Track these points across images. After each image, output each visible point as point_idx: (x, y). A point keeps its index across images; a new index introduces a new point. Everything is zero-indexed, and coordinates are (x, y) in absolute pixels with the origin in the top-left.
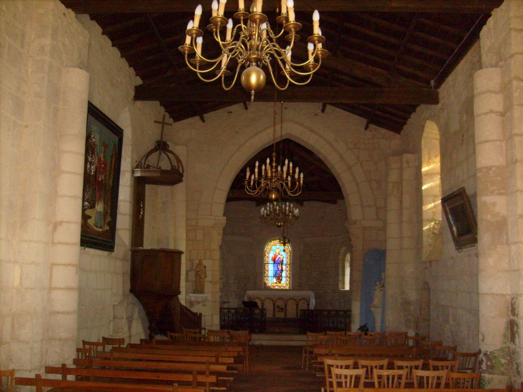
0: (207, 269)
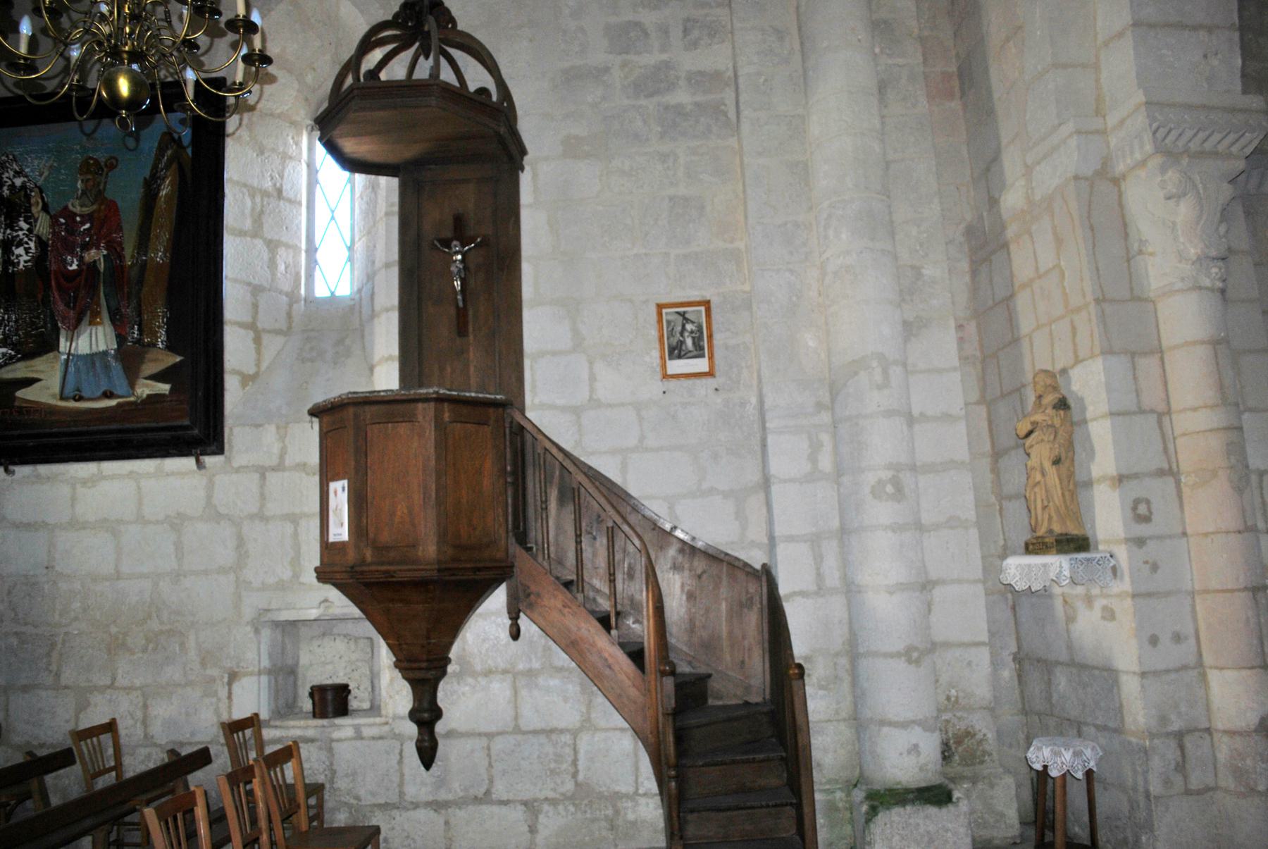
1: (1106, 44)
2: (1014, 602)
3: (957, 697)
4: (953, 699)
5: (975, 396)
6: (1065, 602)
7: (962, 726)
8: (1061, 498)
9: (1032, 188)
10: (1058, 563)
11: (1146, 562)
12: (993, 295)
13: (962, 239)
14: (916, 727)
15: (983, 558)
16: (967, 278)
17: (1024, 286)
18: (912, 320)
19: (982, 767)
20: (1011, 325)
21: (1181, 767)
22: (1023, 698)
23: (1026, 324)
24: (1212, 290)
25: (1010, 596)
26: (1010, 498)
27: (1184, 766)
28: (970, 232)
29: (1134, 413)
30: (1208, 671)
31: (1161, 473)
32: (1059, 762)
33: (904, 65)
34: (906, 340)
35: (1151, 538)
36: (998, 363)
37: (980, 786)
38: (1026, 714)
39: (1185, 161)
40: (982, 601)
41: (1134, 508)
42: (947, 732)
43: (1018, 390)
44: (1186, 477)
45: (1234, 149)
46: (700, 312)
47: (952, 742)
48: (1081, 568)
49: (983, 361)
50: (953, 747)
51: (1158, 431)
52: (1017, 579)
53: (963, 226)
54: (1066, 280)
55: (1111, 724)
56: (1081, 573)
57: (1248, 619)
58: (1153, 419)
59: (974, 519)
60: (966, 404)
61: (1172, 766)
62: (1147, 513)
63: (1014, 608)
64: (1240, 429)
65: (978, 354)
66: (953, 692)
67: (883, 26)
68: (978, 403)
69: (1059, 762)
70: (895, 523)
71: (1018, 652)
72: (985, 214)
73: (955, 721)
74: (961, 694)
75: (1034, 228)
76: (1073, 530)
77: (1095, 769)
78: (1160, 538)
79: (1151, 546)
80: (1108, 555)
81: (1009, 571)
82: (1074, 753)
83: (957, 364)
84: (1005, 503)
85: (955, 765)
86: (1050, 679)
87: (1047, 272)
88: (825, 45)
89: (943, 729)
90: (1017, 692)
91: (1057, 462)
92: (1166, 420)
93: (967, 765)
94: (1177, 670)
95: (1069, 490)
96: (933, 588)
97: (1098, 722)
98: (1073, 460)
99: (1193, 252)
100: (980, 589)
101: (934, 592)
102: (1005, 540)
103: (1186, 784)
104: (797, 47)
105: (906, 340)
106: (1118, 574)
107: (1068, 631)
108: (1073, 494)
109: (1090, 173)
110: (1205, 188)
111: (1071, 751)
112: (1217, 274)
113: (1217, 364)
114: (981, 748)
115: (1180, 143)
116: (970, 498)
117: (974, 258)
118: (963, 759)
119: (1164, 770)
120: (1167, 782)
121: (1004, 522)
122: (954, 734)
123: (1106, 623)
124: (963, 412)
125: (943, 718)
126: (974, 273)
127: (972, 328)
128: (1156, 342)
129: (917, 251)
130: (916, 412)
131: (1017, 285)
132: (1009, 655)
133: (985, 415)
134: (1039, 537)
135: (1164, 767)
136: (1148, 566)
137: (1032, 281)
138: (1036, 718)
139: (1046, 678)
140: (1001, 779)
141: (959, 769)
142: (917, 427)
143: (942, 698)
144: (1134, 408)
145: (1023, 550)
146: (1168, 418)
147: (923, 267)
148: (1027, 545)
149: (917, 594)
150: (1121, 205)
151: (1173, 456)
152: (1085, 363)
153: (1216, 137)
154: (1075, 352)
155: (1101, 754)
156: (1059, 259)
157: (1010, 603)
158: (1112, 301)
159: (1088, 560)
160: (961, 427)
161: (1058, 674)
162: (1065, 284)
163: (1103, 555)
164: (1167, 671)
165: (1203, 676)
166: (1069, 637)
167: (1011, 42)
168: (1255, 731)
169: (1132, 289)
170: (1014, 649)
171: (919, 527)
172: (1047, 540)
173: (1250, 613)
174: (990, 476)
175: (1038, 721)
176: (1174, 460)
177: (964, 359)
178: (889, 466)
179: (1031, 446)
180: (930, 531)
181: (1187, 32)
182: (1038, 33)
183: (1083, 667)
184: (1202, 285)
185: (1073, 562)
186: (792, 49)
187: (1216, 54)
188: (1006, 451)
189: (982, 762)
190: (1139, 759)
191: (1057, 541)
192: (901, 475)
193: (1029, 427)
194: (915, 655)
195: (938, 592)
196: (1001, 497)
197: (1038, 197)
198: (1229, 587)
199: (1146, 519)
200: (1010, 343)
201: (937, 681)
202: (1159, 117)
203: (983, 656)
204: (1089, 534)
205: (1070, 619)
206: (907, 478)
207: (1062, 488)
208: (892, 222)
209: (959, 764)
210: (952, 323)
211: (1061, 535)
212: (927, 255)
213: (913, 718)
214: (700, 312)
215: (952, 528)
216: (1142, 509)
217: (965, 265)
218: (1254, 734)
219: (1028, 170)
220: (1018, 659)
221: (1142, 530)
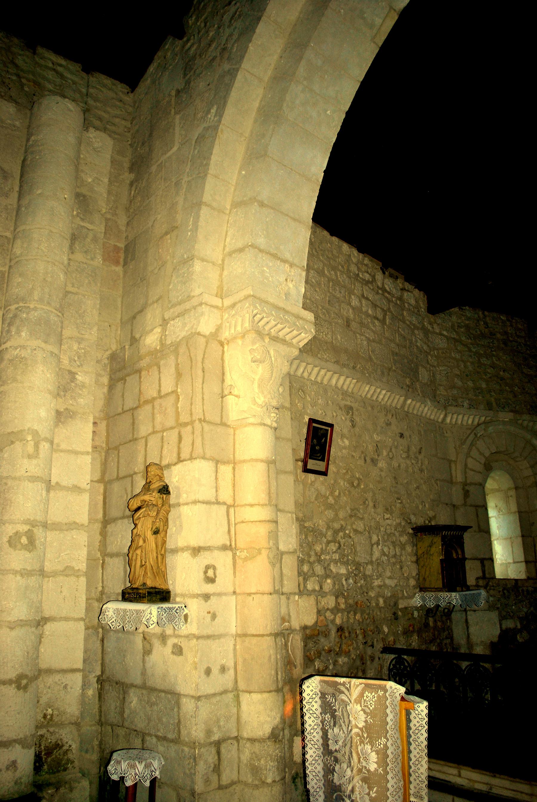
0: (173, 499)
1: (230, 254)
2: (103, 636)
3: (52, 715)
4: (49, 717)
5: (97, 476)
6: (145, 638)
7: (52, 739)
8: (156, 559)
9: (166, 336)
10: (149, 610)
11: (209, 613)
12: (123, 405)
13: (106, 361)
14: (17, 745)
15: (87, 599)
16: (105, 390)
17: (147, 402)
18: (62, 410)
19: (66, 773)
20: (133, 428)
21: (217, 769)
22: (100, 712)
23: (144, 430)
24: (271, 427)
25: (100, 630)
26: (112, 555)
27: (219, 768)
28: (113, 357)
29: (213, 503)
30: (241, 693)
31: (224, 548)
32: (133, 774)
33: (92, 230)
34: (56, 425)
35: (214, 594)
36: (118, 454)
37: (62, 790)
38: (102, 725)
39: (267, 340)
40: (81, 636)
41: (206, 572)
42: (40, 745)
43: (131, 476)
44: (240, 552)
45: (295, 341)
46: (328, 430)
47: (43, 753)
48: (165, 615)
49: (107, 452)
50: (44, 757)
51: (226, 518)
52: (113, 620)
53: (109, 352)
54: (180, 403)
55: (170, 736)
56: (164, 619)
57: (270, 657)
58: (224, 508)
59: (85, 571)
60: (92, 481)
61: (211, 769)
62: (213, 576)
63: (102, 641)
64: (276, 522)
65: (104, 445)
66: (50, 711)
67: (81, 198)
68: (98, 481)
69: (133, 774)
70: (24, 569)
71: (102, 675)
72: (127, 347)
73: (48, 735)
74: (56, 712)
75: (162, 362)
76: (159, 584)
77: (159, 777)
78: (220, 595)
79: (213, 600)
80: (183, 606)
81: (107, 613)
82: (145, 765)
83: (90, 450)
84: (107, 559)
85: (44, 773)
86: (124, 698)
87: (167, 394)
88: (39, 192)
89: (37, 743)
90: (97, 706)
91: (156, 532)
92: (232, 510)
93: (54, 773)
94: (221, 693)
95: (161, 555)
96: (46, 623)
97: (160, 734)
98: (166, 532)
99: (261, 400)
100: (81, 626)
101: (45, 627)
102: (103, 587)
103: (219, 781)
104: (17, 188)
105: (56, 425)
106: (189, 620)
107: (144, 661)
108: (163, 556)
109: (208, 333)
110: (276, 360)
111: (144, 763)
112: (275, 417)
113: (269, 476)
114: (66, 757)
115: (267, 328)
116: (83, 553)
117: (113, 376)
118: (50, 767)
119: (206, 772)
120: (207, 781)
121: (104, 573)
122: (45, 747)
123: (175, 656)
124: (88, 487)
125: (39, 734)
126: (111, 387)
127: (103, 426)
128: (232, 456)
129: (75, 361)
130: (53, 483)
131: (142, 400)
132: (95, 677)
133: (102, 490)
134: (135, 588)
135: (205, 769)
136: (210, 615)
137: (154, 399)
138: (109, 728)
139: (121, 697)
140: (79, 783)
141: (47, 776)
142: (52, 494)
143: (40, 717)
144: (213, 500)
145: (120, 598)
146: (233, 509)
147: (77, 374)
148: (124, 593)
149: (34, 629)
150: (223, 360)
151: (233, 536)
152: (185, 462)
153: (287, 330)
154: (179, 454)
155: (163, 763)
156: (177, 388)
157: (100, 636)
158: (209, 423)
159: (170, 609)
160: (86, 497)
161: (131, 694)
162: (179, 405)
163: (180, 606)
164: (214, 695)
165: (237, 697)
166: (144, 666)
167: (169, 236)
168: (269, 738)
169: (222, 418)
170: (99, 673)
171: (42, 573)
172: (141, 591)
173: (272, 652)
174: (98, 538)
175: (110, 731)
176: (233, 540)
177: (94, 447)
178: (27, 522)
179: (139, 518)
180: (49, 577)
181: (279, 261)
182: (189, 234)
183: (153, 690)
184: (266, 423)
185: (159, 610)
186: (13, 188)
187: (292, 281)
188: (115, 520)
189: (65, 769)
190: (189, 764)
191: (149, 593)
192: (35, 530)
193: (139, 504)
194: (24, 682)
195: (48, 628)
196: (105, 554)
197: (168, 342)
198: (261, 633)
199: (211, 580)
200: (130, 441)
201: (38, 702)
202: (259, 307)
203: (79, 677)
204: (171, 588)
205: (147, 652)
206: (39, 532)
207: (157, 553)
208: (61, 335)
209: (47, 773)
210: (91, 419)
211: (152, 588)
212: (82, 365)
213: (15, 738)
214: (328, 430)
215: (67, 576)
216: (210, 573)
217: (105, 380)
218: (267, 741)
219: (165, 323)
220: (100, 680)
221: (209, 588)
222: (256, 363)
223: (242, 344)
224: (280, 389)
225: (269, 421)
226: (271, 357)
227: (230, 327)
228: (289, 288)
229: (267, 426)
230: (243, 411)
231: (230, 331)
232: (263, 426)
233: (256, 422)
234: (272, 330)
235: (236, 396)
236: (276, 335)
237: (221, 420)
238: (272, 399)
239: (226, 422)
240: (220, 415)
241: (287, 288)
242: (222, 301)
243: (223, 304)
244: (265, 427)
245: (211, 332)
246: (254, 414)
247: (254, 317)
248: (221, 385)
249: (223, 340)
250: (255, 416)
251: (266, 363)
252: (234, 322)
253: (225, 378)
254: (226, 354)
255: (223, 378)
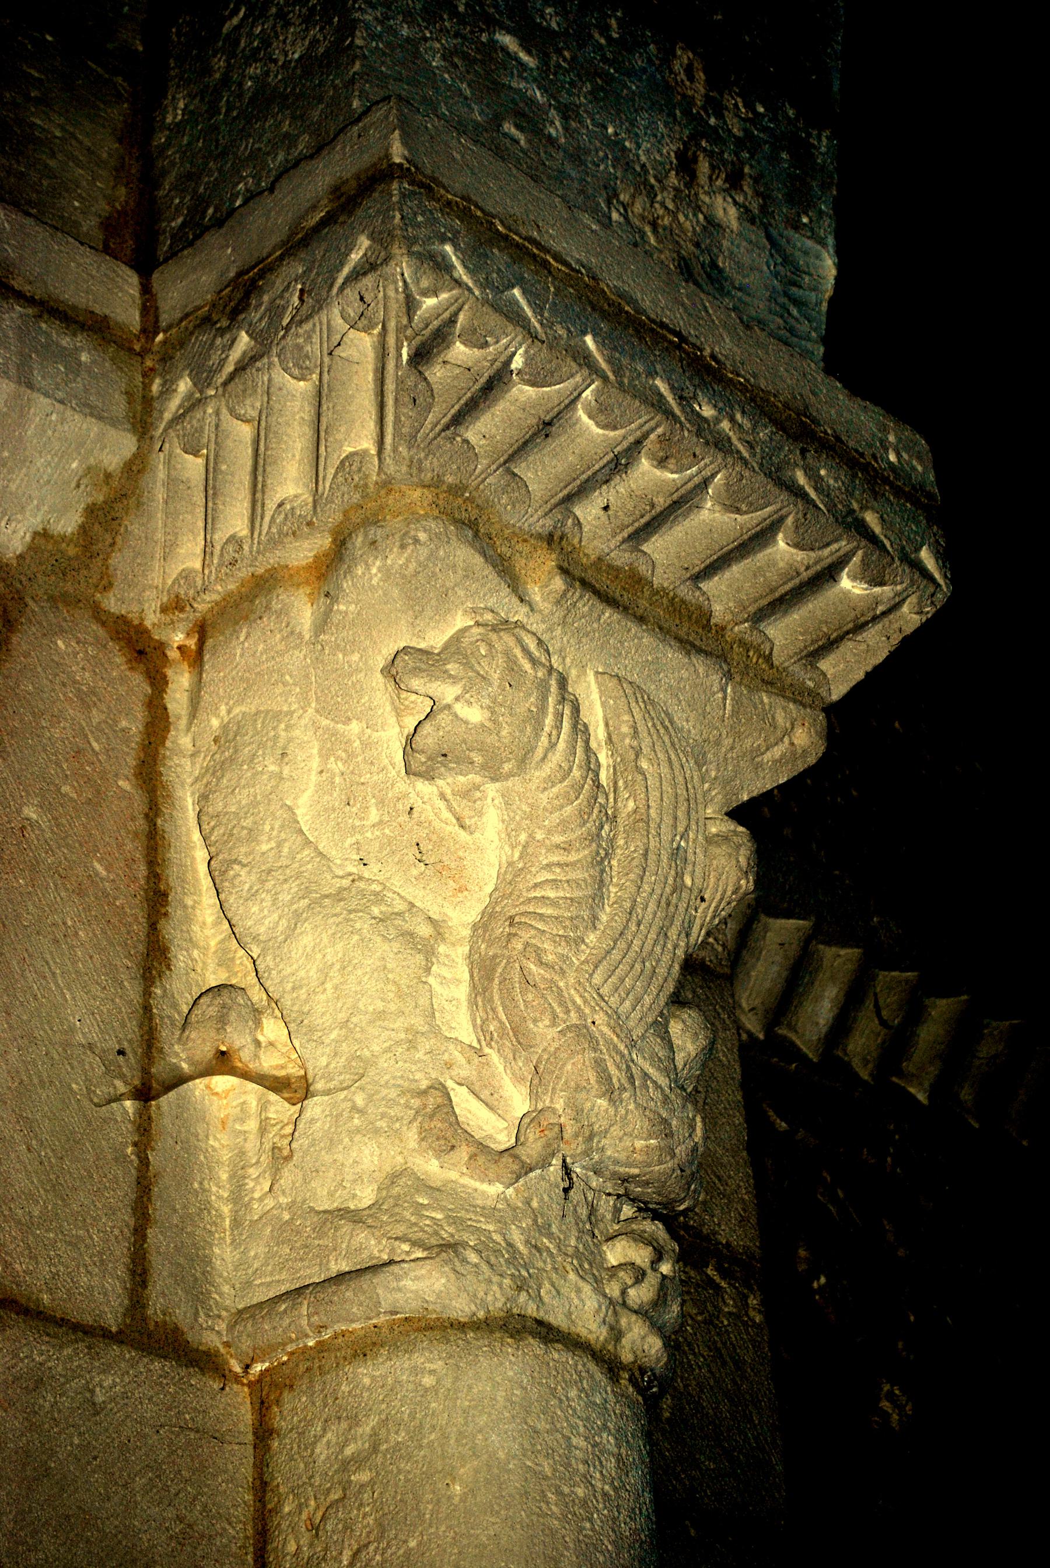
184: (557, 1319)
222: (448, 782)
223: (322, 625)
224: (675, 1028)
225: (590, 1301)
226: (581, 730)
227: (211, 488)
228: (712, 225)
229: (574, 1343)
230: (344, 1213)
231: (210, 521)
232: (535, 1346)
233: (462, 1308)
234: (588, 512)
235: (277, 1085)
236: (622, 558)
237: (137, 1301)
238: (610, 1092)
239: (181, 1315)
240: (121, 1251)
241: (689, 222)
242: (146, 289)
243: (149, 307)
244: (558, 1354)
245: (44, 534)
246: (448, 1232)
247: (421, 356)
248: (133, 990)
249: (151, 618)
250: (451, 1248)
251: (538, 775)
252: (245, 431)
253: (169, 930)
254: (181, 739)
255: (153, 927)
